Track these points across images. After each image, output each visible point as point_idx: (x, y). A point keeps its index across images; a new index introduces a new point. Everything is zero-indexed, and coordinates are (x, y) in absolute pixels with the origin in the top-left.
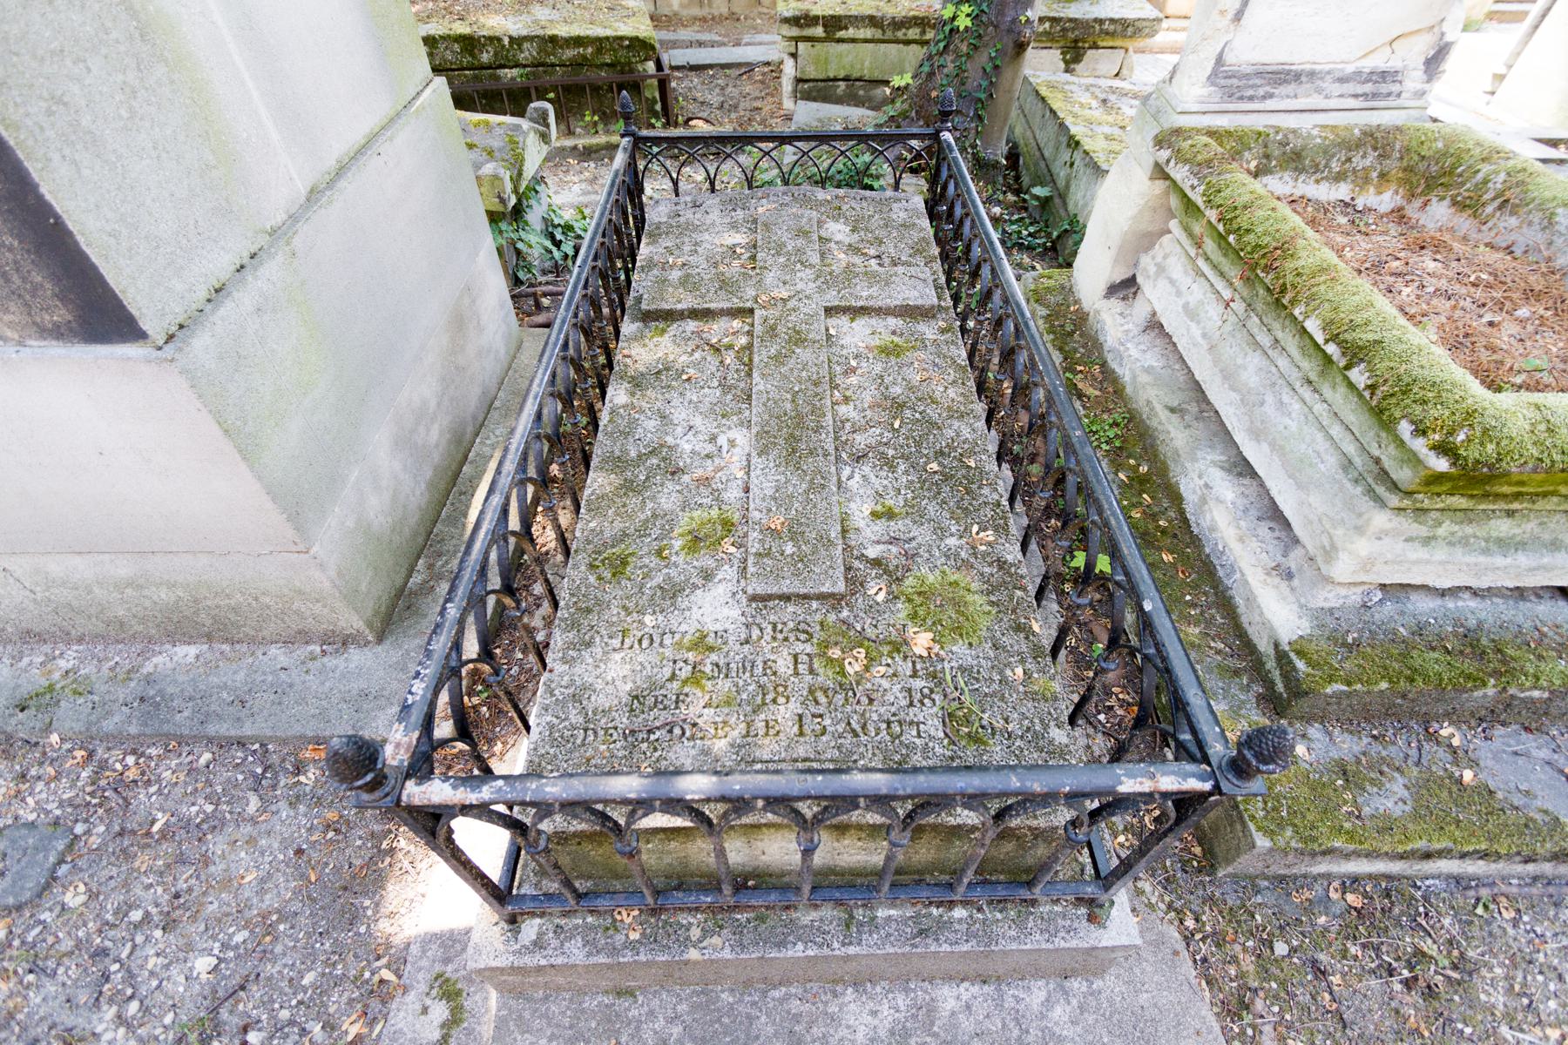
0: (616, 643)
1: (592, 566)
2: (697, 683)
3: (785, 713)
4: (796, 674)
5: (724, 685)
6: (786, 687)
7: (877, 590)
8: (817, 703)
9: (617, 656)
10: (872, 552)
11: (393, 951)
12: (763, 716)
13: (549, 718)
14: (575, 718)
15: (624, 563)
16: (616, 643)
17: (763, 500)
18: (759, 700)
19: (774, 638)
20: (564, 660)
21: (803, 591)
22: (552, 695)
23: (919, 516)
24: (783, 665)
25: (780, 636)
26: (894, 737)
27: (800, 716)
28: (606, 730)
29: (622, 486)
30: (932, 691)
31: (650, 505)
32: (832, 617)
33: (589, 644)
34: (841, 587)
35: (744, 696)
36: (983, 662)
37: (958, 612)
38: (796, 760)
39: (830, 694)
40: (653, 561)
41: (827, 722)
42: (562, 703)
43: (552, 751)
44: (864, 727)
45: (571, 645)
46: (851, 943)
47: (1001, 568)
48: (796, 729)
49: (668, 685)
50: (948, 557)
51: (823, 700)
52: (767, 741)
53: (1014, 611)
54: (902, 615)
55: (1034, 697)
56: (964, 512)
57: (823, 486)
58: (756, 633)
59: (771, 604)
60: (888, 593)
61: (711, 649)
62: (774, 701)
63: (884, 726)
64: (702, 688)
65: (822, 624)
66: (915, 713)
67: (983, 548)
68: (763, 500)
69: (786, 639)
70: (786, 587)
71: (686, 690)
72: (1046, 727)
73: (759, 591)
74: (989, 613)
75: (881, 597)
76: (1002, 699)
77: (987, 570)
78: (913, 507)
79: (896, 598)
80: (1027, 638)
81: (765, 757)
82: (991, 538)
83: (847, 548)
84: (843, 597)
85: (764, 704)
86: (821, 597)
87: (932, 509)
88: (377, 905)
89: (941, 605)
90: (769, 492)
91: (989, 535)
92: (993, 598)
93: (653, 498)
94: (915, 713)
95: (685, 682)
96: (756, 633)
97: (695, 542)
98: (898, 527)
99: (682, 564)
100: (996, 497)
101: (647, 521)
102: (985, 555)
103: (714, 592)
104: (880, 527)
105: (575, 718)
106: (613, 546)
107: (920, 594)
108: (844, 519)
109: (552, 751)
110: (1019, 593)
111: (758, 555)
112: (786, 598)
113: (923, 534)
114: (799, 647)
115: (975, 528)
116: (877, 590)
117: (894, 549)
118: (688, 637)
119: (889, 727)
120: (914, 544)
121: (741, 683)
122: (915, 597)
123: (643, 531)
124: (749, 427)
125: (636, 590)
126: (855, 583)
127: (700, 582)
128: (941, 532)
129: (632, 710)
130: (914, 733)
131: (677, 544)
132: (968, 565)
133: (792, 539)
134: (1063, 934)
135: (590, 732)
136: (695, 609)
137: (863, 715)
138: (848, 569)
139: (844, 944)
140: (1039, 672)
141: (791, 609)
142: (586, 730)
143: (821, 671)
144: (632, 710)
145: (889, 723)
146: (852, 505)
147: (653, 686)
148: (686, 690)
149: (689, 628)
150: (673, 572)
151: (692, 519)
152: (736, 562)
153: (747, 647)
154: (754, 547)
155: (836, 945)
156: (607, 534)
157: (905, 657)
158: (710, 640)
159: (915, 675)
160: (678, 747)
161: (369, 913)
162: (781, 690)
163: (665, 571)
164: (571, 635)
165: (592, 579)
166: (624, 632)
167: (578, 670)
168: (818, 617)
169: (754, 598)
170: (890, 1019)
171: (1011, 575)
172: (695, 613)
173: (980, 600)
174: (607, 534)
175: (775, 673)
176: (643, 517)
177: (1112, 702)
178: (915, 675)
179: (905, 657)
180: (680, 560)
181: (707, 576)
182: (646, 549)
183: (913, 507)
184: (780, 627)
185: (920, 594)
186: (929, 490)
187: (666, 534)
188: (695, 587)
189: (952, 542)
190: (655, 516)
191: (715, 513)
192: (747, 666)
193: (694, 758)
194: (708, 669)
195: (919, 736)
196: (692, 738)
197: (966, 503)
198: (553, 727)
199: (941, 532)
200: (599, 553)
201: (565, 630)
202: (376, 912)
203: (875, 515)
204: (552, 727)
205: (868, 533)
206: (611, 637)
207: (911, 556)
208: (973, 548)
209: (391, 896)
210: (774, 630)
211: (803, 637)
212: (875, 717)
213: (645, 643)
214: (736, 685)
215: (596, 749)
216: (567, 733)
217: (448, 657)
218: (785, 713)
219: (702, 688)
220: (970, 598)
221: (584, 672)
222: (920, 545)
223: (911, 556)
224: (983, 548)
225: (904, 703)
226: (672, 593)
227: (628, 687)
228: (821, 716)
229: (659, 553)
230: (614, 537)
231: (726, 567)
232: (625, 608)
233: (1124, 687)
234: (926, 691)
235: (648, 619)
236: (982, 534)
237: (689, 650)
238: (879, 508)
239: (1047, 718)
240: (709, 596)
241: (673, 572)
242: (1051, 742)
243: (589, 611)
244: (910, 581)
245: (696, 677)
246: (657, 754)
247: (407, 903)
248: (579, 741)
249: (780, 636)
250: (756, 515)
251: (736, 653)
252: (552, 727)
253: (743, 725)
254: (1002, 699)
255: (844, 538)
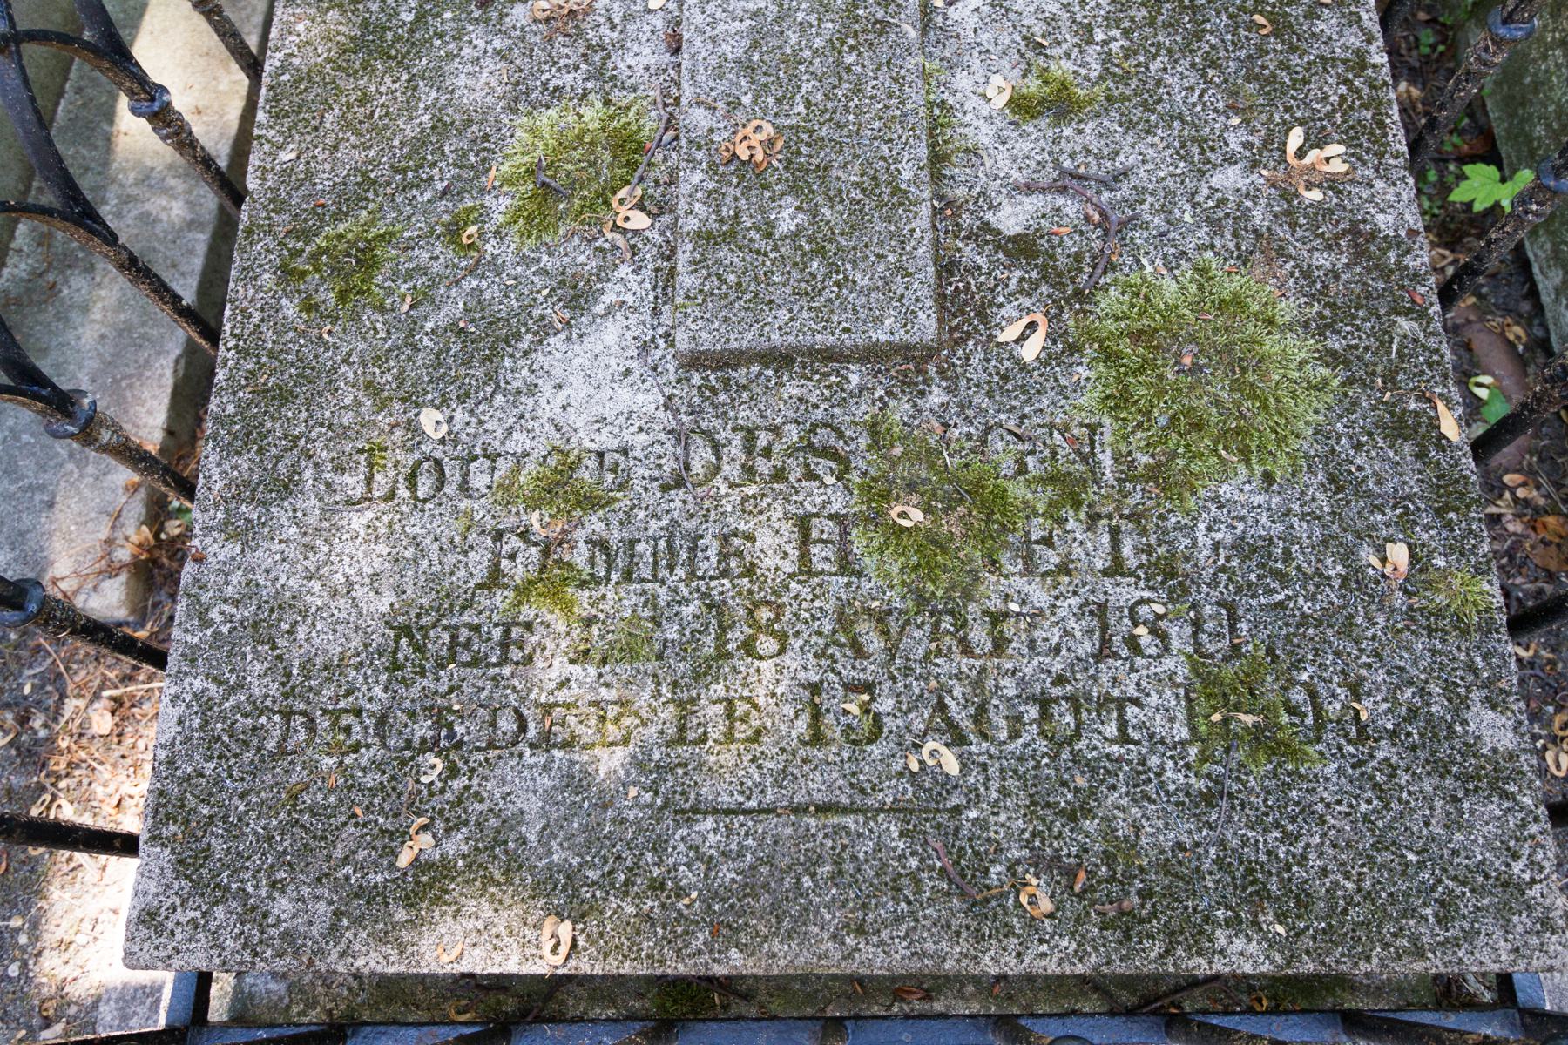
1: (287, 273)
2: (555, 595)
3: (771, 680)
4: (806, 570)
5: (620, 600)
6: (779, 609)
7: (1022, 331)
8: (859, 651)
9: (356, 522)
10: (1011, 219)
11: (73, 1010)
12: (718, 690)
13: (198, 684)
14: (263, 686)
15: (367, 262)
16: (352, 483)
17: (718, 73)
18: (709, 643)
19: (749, 471)
20: (232, 530)
21: (823, 340)
22: (205, 622)
23: (1134, 99)
24: (772, 546)
25: (763, 466)
26: (1058, 743)
27: (815, 688)
29: (358, 43)
31: (428, 96)
32: (901, 409)
33: (288, 487)
34: (927, 326)
35: (672, 633)
36: (1301, 528)
37: (1237, 386)
38: (800, 810)
40: (437, 257)
41: (885, 705)
42: (227, 645)
44: (980, 715)
45: (242, 491)
47: (1359, 253)
48: (802, 725)
49: (483, 600)
50: (1216, 226)
51: (874, 643)
52: (728, 759)
53: (1390, 379)
54: (1086, 399)
55: (1431, 622)
56: (1267, 91)
57: (882, 27)
58: (701, 457)
59: (740, 375)
60: (1051, 337)
61: (591, 502)
62: (748, 647)
63: (1033, 712)
64: (568, 607)
65: (873, 429)
66: (1114, 677)
67: (1315, 195)
68: (718, 73)
69: (779, 475)
70: (780, 327)
72: (1459, 704)
73: (707, 341)
74: (1322, 386)
75: (1031, 350)
76: (1347, 629)
77: (1321, 259)
78: (1125, 78)
79: (1073, 349)
80: (1420, 456)
81: (725, 800)
82: (1338, 167)
83: (946, 208)
84: (929, 353)
85: (723, 654)
86: (872, 355)
87: (1178, 83)
88: (35, 924)
89: (1196, 368)
90: (733, 49)
91: (1333, 157)
92: (1335, 343)
93: (435, 76)
94: (1114, 677)
95: (524, 591)
96: (701, 457)
97: (546, 198)
98: (1081, 139)
100: (1354, 39)
101: (421, 141)
102: (1321, 213)
103: (593, 344)
104: (1031, 142)
105: (263, 686)
106: (338, 217)
107: (1137, 336)
108: (939, 119)
110: (1405, 325)
111: (705, 237)
112: (781, 359)
113: (1148, 160)
114: (813, 498)
115: (1296, 138)
116: (1022, 331)
117: (1071, 208)
118: (531, 468)
119: (1045, 715)
120: (1125, 190)
121: (664, 596)
122: (1125, 346)
123: (411, 169)
124: (1468, 73)
125: (398, 337)
126: (964, 310)
127: (556, 314)
128: (1200, 151)
129: (396, 666)
130: (1111, 730)
131: (500, 207)
132: (1267, 247)
133: (794, 189)
136: (547, 389)
137: (978, 683)
138: (946, 268)
140: (1449, 551)
141: (792, 390)
142: (287, 714)
143: (870, 563)
144: (396, 666)
145: (1045, 702)
146: (962, 81)
147: (448, 602)
148: (527, 613)
149: (532, 442)
150: (490, 288)
152: (649, 254)
153: (678, 495)
154: (695, 216)
156: (323, 182)
157: (1094, 518)
158: (585, 474)
159: (1116, 568)
160: (507, 769)
161: (23, 939)
162: (767, 617)
165: (290, 308)
166: (373, 453)
167: (263, 556)
168: (864, 409)
169: (694, 361)
171: (1386, 274)
172: (548, 403)
173: (1299, 348)
174: (323, 182)
175: (750, 571)
176: (410, 130)
177: (1503, 507)
178: (1116, 568)
179: (1094, 518)
180: (504, 251)
181: (577, 296)
182: (419, 223)
183: (1125, 78)
184: (763, 439)
185: (1137, 336)
186: (1171, 25)
187: (472, 176)
188: (545, 329)
189: (1229, 179)
191: (592, 115)
192: (680, 548)
193: (548, 796)
194: (580, 556)
195: (1123, 738)
197: (1271, 61)
198: (207, 706)
199: (1200, 151)
200: (306, 235)
201: (228, 451)
202: (35, 938)
203: (1022, 106)
204: (206, 706)
205: (1001, 161)
206: (340, 469)
208: (1288, 195)
209: (58, 909)
210: (749, 449)
211: (823, 466)
212: (1009, 688)
213: (424, 487)
214: (651, 602)
215: (313, 768)
216: (243, 723)
217: (115, 427)
218: (771, 680)
219: (568, 607)
220: (1271, 344)
221: (276, 561)
222: (1141, 191)
224: (1315, 195)
225: (1086, 647)
226: (488, 348)
227: (383, 604)
228: (868, 687)
230: (340, 192)
231: (624, 271)
232: (372, 388)
233: (1531, 472)
235: (429, 419)
236: (1313, 155)
237: (533, 504)
238: (1033, 86)
239: (1462, 680)
240: (580, 355)
241: (490, 288)
242: (1471, 748)
243: (285, 396)
244: (1111, 300)
245: (553, 578)
246: (457, 784)
248: (271, 745)
251: (652, 513)
252: (206, 706)
253: (669, 712)
254: (1347, 629)
255: (936, 178)
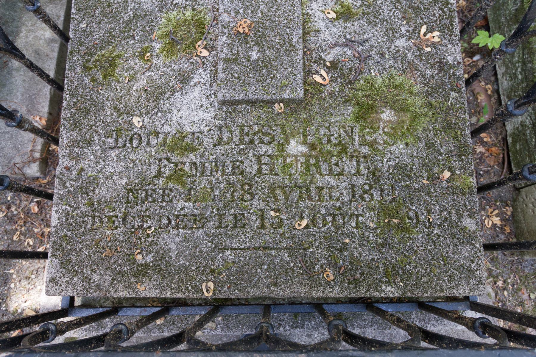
0: (111, 141)
1: (86, 68)
6: (251, 186)
9: (113, 154)
15: (113, 65)
16: (111, 141)
22: (65, 187)
28: (110, 218)
30: (371, 187)
35: (217, 193)
39: (288, 190)
40: (137, 64)
43: (69, 234)
46: (297, 327)
47: (441, 69)
48: (258, 222)
49: (156, 181)
67: (429, 49)
69: (252, 142)
70: (253, 92)
71: (171, 185)
72: (460, 217)
73: (228, 97)
76: (428, 194)
77: (429, 72)
82: (437, 40)
85: (233, 200)
99: (163, 67)
101: (129, 22)
102: (430, 55)
103: (190, 96)
106: (102, 48)
108: (306, 19)
109: (69, 234)
111: (227, 60)
112: (252, 103)
113: (375, 36)
115: (424, 29)
119: (334, 220)
120: (367, 46)
121: (214, 181)
125: (124, 92)
127: (179, 85)
128: (392, 33)
129: (128, 202)
130: (354, 224)
132: (412, 67)
133: (257, 44)
134: (433, 322)
135: (97, 220)
136: (175, 111)
139: (292, 327)
140: (461, 168)
142: (94, 217)
144: (128, 202)
145: (334, 216)
148: (171, 185)
151: (169, 20)
153: (219, 148)
155: (287, 328)
163: (148, 73)
164: (74, 134)
165: (87, 80)
169: (223, 103)
170: (318, 338)
172: (175, 116)
175: (242, 173)
176: (126, 17)
181: (185, 79)
184: (246, 130)
187: (147, 35)
188: (173, 91)
189: (401, 43)
190: (136, 16)
193: (178, 244)
196: (177, 227)
199: (392, 33)
200: (91, 55)
207: (362, 59)
214: (211, 183)
215: (103, 234)
222: (372, 46)
223: (362, 59)
224: (429, 49)
225: (347, 198)
227: (124, 182)
229: (142, 55)
234: (367, 187)
235: (136, 120)
236: (429, 35)
239: (462, 209)
240: (186, 99)
241: (155, 75)
243: (87, 111)
247: (35, 272)
248: (89, 227)
249: (247, 139)
250: (225, 18)
254: (428, 194)
255: (304, 40)
